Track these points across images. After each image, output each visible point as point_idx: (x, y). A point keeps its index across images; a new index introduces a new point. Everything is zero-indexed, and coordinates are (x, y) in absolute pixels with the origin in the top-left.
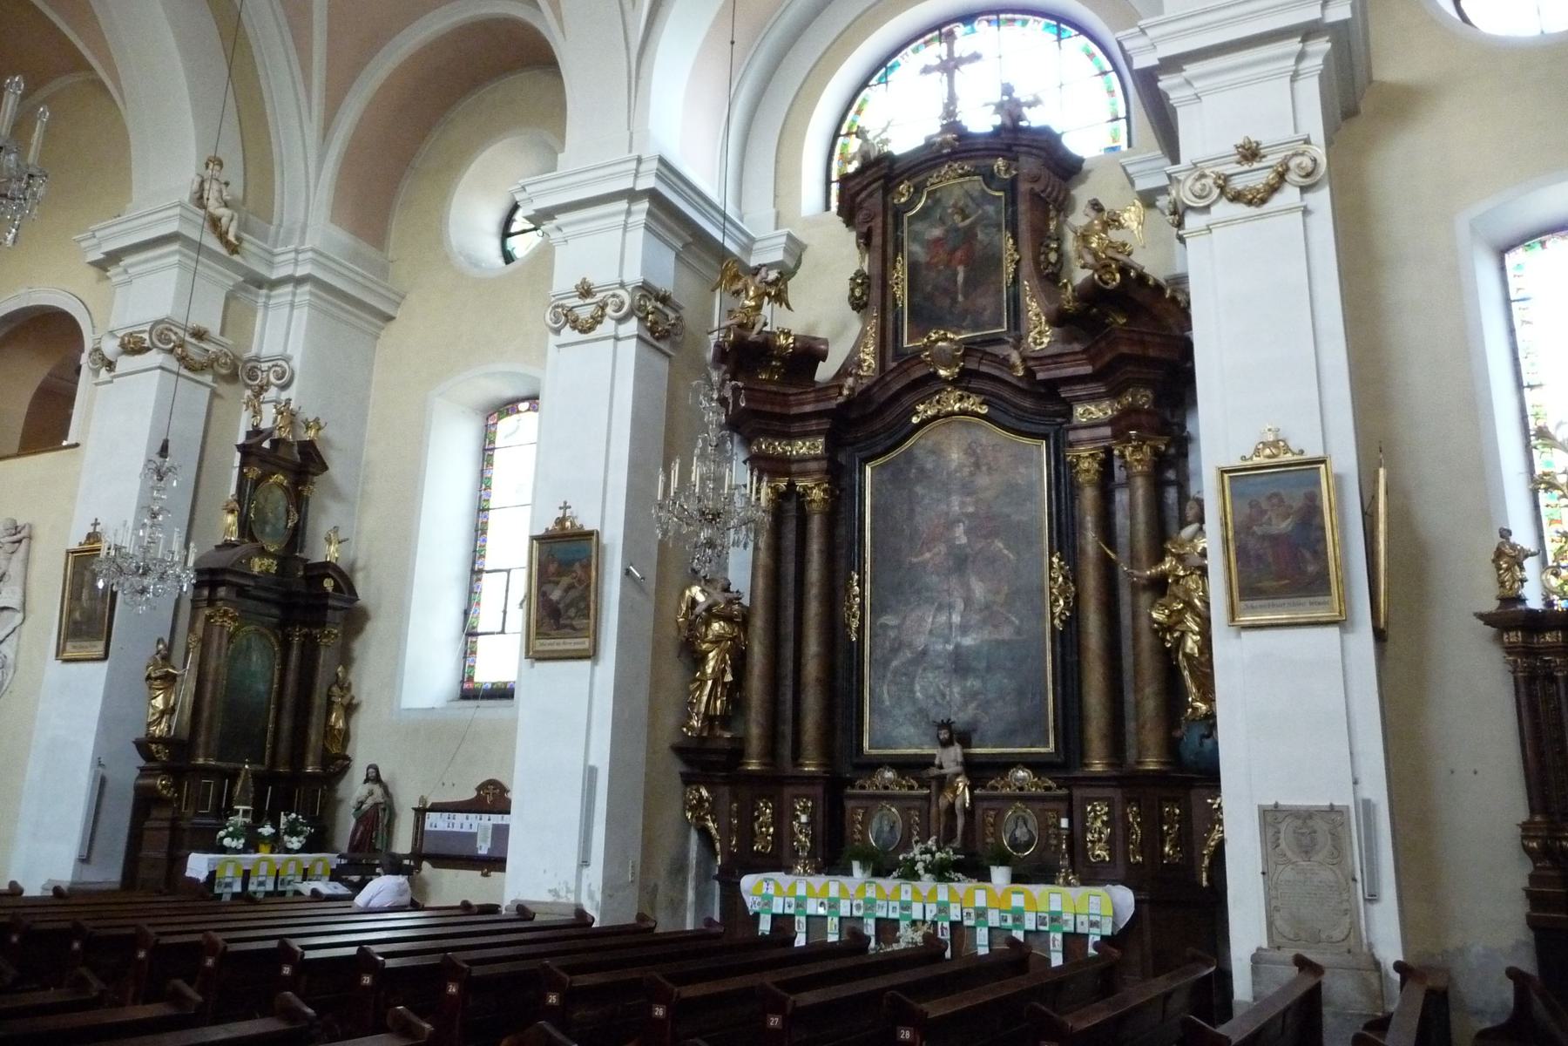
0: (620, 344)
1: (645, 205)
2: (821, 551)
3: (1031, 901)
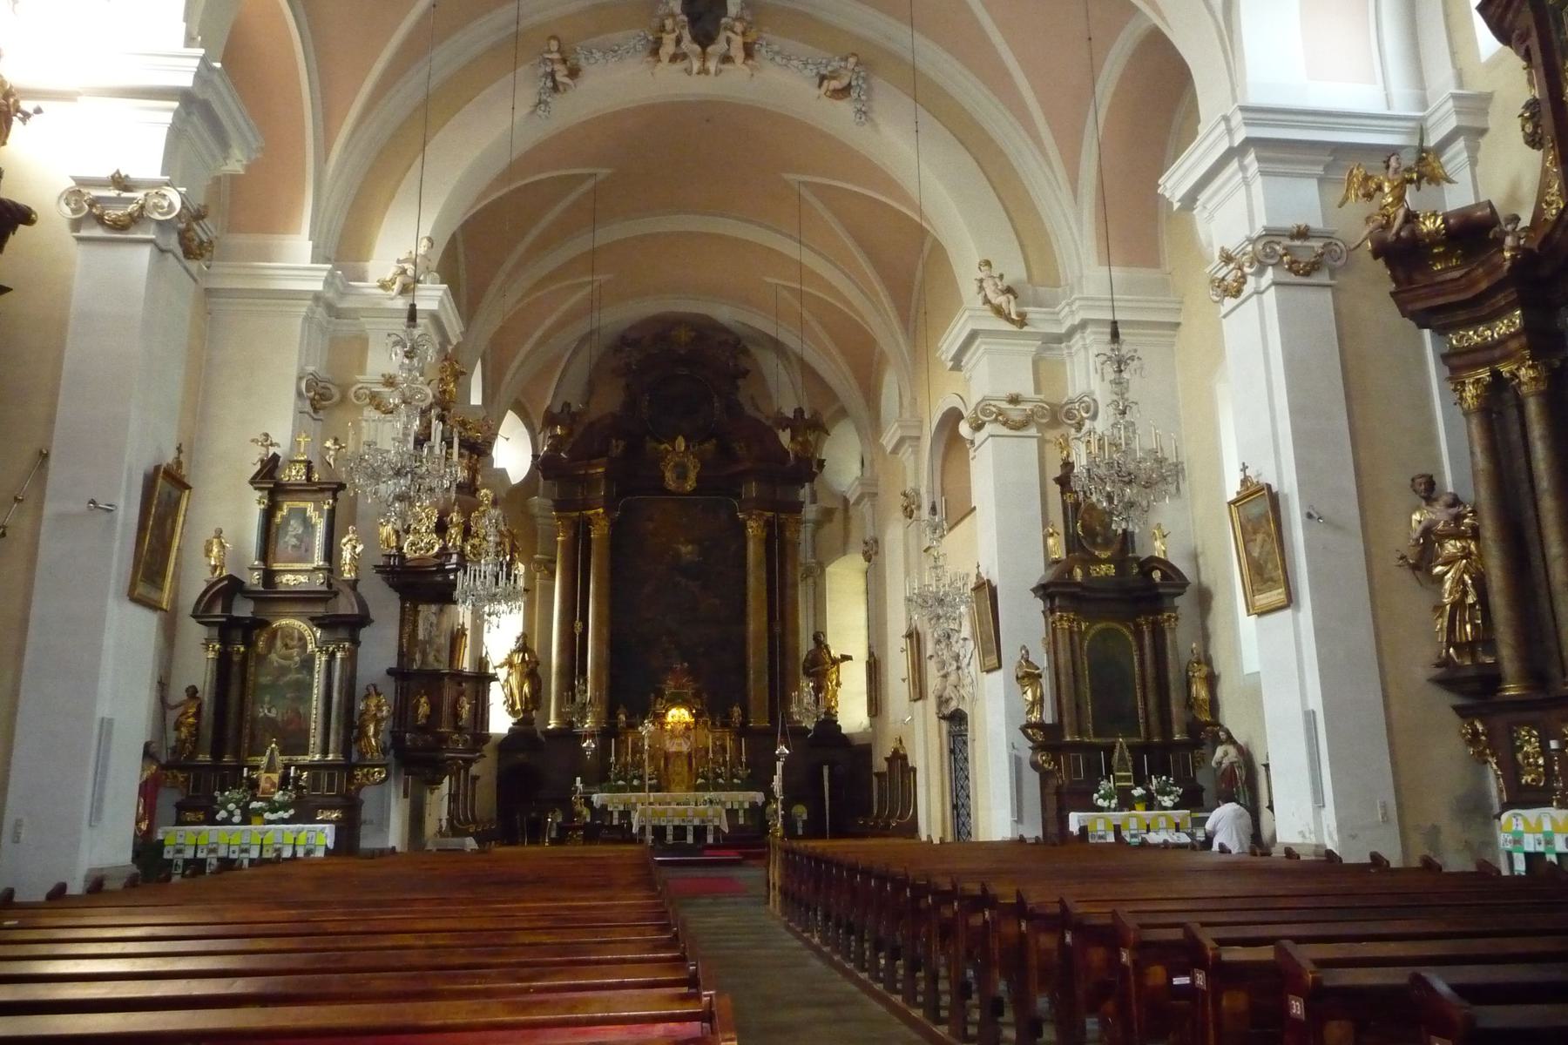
0: (1265, 296)
1: (1251, 158)
2: (1543, 437)
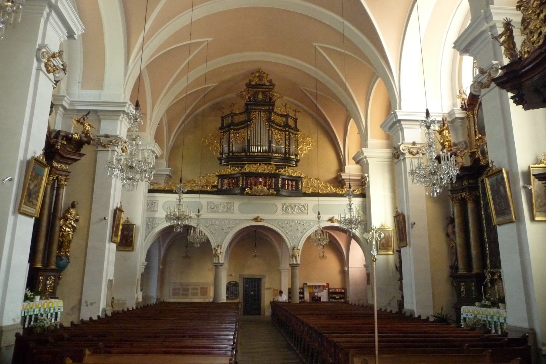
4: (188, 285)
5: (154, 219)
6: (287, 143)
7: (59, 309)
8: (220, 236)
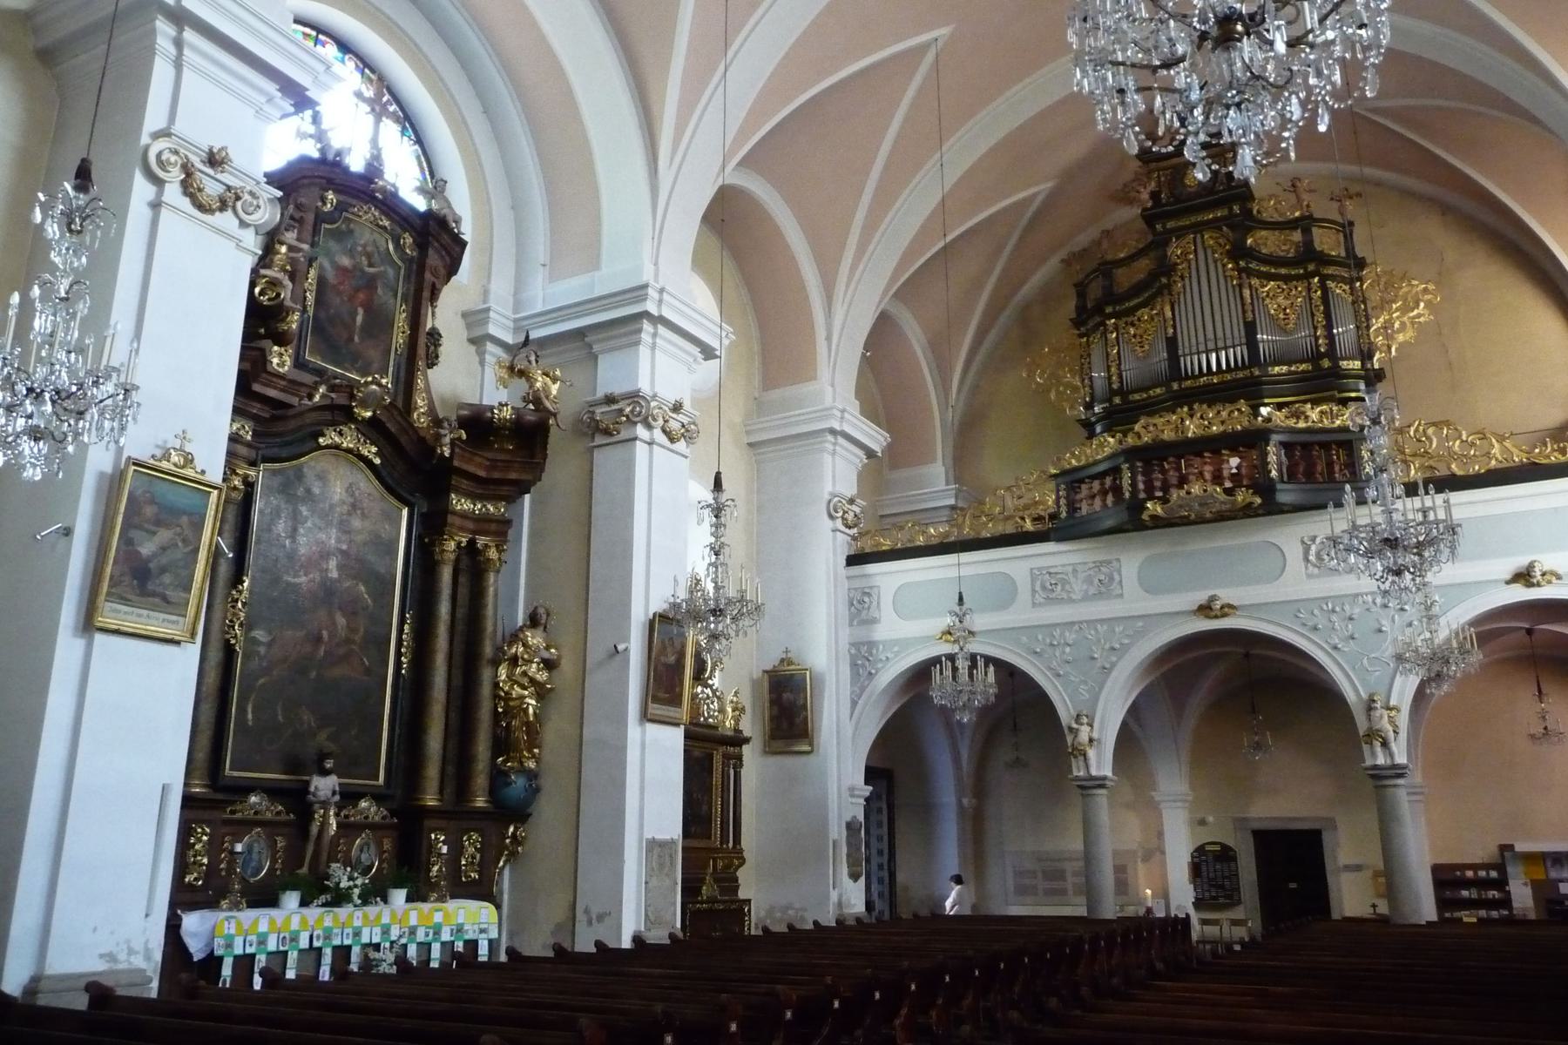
3: (447, 915)
4: (1059, 860)
5: (871, 645)
6: (1320, 317)
7: (482, 931)
8: (1085, 683)
